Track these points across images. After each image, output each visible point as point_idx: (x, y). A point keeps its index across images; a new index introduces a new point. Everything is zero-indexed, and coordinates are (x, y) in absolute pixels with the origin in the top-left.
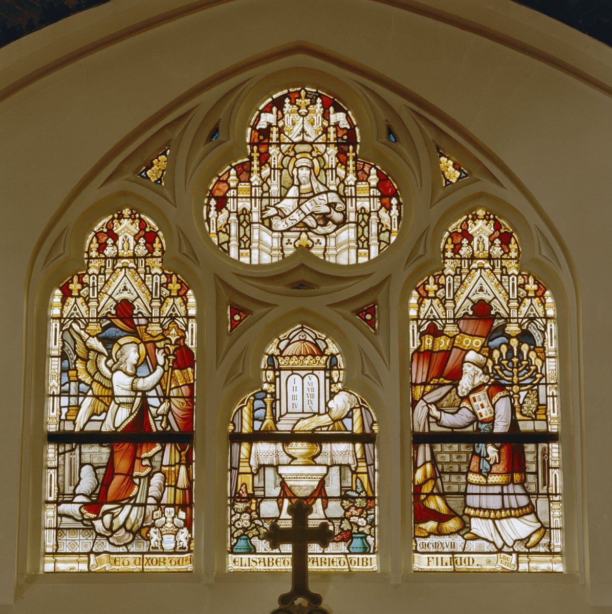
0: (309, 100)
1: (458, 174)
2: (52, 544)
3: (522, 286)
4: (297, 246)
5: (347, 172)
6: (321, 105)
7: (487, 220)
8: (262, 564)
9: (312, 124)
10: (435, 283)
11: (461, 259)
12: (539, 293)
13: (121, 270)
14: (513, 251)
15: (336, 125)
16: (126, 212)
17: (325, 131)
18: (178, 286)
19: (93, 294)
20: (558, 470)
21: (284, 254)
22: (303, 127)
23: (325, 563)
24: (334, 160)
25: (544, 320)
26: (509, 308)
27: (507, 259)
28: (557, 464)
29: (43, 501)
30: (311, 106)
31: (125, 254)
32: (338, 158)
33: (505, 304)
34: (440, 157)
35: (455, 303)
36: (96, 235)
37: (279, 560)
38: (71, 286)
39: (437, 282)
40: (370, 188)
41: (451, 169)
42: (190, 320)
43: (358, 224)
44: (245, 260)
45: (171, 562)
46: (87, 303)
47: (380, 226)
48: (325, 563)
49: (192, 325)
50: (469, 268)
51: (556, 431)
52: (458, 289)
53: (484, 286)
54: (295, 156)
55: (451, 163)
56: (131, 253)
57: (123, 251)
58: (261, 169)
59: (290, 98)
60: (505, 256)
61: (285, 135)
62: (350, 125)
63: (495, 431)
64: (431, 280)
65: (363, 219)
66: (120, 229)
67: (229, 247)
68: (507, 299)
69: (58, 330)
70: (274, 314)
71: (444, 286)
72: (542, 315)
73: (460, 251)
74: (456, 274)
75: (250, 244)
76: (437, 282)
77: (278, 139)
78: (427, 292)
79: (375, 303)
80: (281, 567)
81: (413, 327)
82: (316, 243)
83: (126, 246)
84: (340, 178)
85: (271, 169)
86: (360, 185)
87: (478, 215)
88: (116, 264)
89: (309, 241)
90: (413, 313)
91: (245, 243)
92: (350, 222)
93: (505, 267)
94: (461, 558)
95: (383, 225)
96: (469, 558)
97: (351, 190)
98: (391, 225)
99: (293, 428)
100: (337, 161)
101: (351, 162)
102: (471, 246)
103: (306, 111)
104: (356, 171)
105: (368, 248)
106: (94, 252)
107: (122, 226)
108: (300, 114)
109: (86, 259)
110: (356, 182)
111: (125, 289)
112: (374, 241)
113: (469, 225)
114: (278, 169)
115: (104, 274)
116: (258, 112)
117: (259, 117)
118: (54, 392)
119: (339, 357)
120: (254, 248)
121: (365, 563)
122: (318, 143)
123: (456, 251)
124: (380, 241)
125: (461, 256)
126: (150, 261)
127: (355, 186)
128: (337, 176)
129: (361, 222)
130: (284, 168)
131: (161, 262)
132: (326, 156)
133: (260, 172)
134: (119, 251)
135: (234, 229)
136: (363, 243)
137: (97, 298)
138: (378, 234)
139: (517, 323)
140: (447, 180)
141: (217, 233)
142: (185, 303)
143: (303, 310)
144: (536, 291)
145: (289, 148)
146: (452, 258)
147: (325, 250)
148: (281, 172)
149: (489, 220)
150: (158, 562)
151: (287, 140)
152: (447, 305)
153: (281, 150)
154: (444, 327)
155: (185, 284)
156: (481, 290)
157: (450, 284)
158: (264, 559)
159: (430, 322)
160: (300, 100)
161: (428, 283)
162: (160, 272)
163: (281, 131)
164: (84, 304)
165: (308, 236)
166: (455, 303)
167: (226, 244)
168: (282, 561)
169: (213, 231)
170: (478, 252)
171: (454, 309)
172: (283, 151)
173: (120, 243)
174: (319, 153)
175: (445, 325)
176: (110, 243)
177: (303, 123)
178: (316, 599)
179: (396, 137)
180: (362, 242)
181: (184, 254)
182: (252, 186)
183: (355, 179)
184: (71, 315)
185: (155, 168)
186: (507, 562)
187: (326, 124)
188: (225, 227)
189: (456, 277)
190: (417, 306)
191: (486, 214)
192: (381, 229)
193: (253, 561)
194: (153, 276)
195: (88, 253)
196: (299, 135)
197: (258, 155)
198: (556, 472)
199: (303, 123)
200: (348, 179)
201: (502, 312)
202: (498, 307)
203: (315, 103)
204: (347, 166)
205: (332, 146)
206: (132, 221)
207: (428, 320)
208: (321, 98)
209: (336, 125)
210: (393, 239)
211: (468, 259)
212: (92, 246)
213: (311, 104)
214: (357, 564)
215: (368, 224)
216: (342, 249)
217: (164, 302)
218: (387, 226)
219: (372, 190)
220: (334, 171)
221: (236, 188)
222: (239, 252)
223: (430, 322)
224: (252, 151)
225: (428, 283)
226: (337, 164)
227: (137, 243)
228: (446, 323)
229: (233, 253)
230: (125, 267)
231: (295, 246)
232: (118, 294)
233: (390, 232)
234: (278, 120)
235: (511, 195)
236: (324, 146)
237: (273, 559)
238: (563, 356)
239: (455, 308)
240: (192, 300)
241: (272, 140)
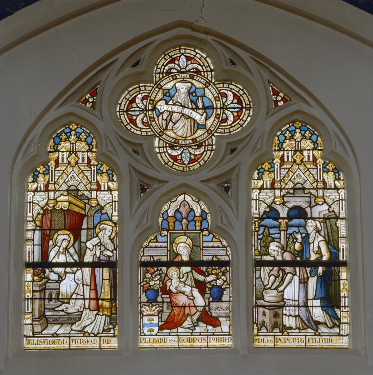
8: (46, 343)
23: (221, 341)
37: (55, 341)
45: (59, 342)
48: (221, 341)
63: (323, 260)
70: (164, 188)
79: (230, 179)
96: (165, 338)
118: (344, 295)
143: (184, 185)
150: (54, 342)
158: (217, 338)
168: (58, 341)
193: (40, 342)
214: (62, 343)
235: (316, 111)
237: (296, 339)
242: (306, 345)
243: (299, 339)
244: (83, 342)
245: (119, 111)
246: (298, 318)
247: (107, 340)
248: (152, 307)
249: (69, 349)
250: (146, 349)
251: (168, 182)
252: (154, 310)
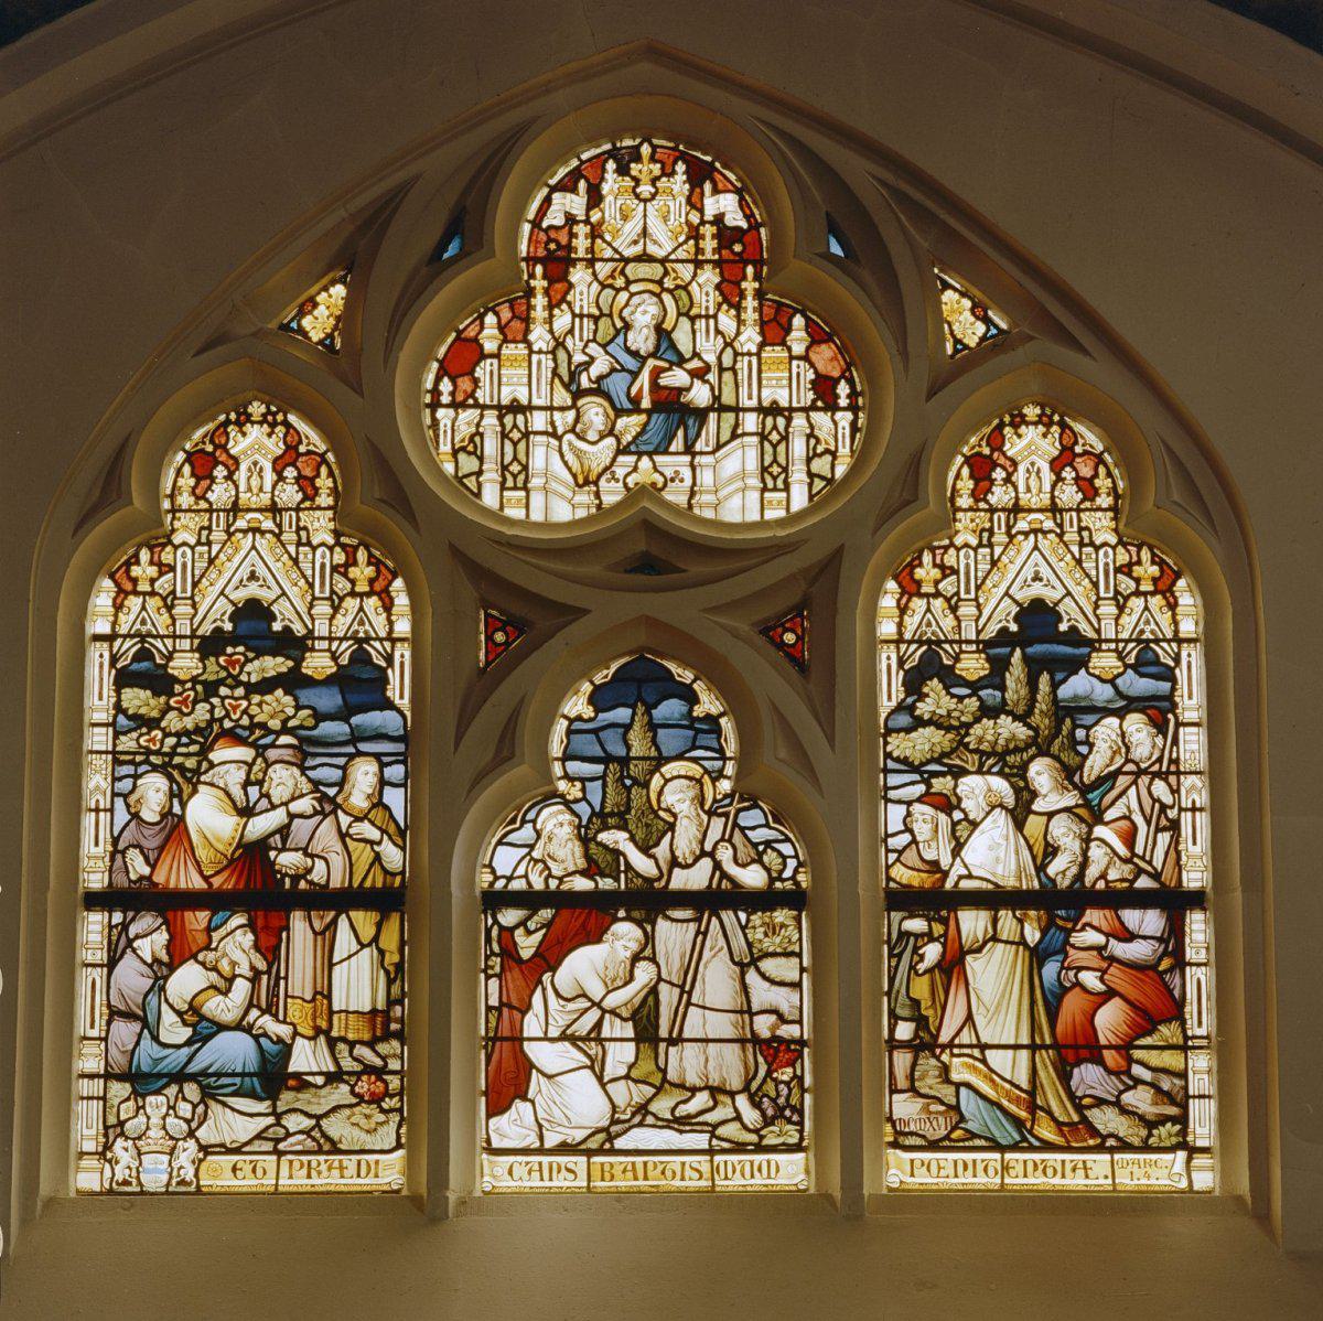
0: (659, 166)
1: (981, 328)
2: (93, 1132)
3: (1126, 569)
4: (631, 485)
5: (740, 322)
6: (684, 177)
7: (1044, 425)
8: (630, 1175)
9: (665, 219)
10: (152, 563)
11: (210, 511)
12: (377, 587)
13: (1026, 538)
14: (324, 491)
15: (719, 219)
16: (257, 409)
17: (694, 234)
18: (370, 571)
19: (968, 591)
20: (1203, 968)
21: (601, 503)
22: (645, 223)
24: (711, 298)
25: (387, 645)
26: (1097, 616)
27: (311, 509)
28: (1202, 957)
30: (664, 179)
31: (255, 502)
32: (722, 294)
33: (1089, 610)
34: (943, 291)
35: (194, 606)
36: (190, 457)
38: (919, 573)
39: (938, 561)
40: (791, 358)
41: (967, 316)
42: (399, 645)
43: (763, 437)
44: (515, 513)
45: (986, 1170)
46: (954, 609)
47: (813, 441)
48: (319, 1173)
49: (402, 656)
50: (1008, 533)
51: (1199, 884)
52: (202, 576)
53: (1041, 570)
54: (626, 288)
55: (967, 303)
56: (265, 499)
57: (249, 495)
58: (551, 316)
59: (617, 161)
60: (1087, 504)
61: (604, 241)
62: (749, 221)
64: (144, 555)
65: (775, 427)
66: (1019, 447)
67: (479, 485)
68: (1094, 598)
69: (894, 667)
71: (172, 569)
72: (383, 634)
73: (989, 497)
74: (980, 545)
75: (526, 481)
76: (938, 561)
77: (591, 250)
78: (135, 581)
81: (889, 658)
82: (672, 480)
83: (255, 482)
84: (724, 337)
85: (574, 315)
86: (768, 352)
87: (251, 415)
88: (235, 521)
89: (657, 475)
90: (887, 628)
91: (515, 477)
92: (744, 434)
93: (1087, 528)
94: (752, 1163)
95: (818, 442)
96: (726, 1162)
97: (750, 362)
98: (836, 441)
100: (720, 299)
101: (750, 303)
102: (234, 482)
103: (653, 190)
104: (763, 325)
105: (787, 488)
106: (185, 494)
107: (1025, 441)
108: (637, 196)
109: (169, 511)
110: (761, 346)
111: (253, 576)
112: (798, 475)
113: (231, 436)
114: (589, 316)
115: (209, 543)
116: (545, 191)
117: (547, 201)
118: (1194, 802)
119: (723, 721)
120: (535, 489)
122: (677, 261)
123: (979, 494)
124: (811, 475)
125: (211, 504)
126: (1088, 519)
127: (758, 354)
128: (718, 332)
129: (770, 433)
130: (602, 315)
131: (334, 519)
132: (694, 288)
133: (550, 320)
134: (241, 495)
135: (490, 446)
136: (775, 478)
137: (192, 598)
138: (809, 460)
139: (1116, 650)
140: (957, 341)
141: (455, 453)
142: (388, 607)
144: (1155, 580)
145: (614, 271)
146: (971, 509)
147: (692, 494)
148: (596, 324)
149: (1048, 425)
151: (609, 253)
152: (961, 611)
153: (594, 274)
154: (957, 659)
155: (386, 567)
156: (1037, 578)
157: (184, 566)
158: (540, 1164)
159: (925, 648)
160: (640, 166)
161: (138, 563)
162: (1113, 540)
163: (595, 233)
164: (948, 612)
165: (654, 463)
166: (194, 606)
167: (473, 478)
169: (445, 448)
170: (1029, 495)
171: (977, 620)
172: (601, 277)
173: (1020, 477)
174: (679, 282)
175: (958, 655)
176: (1069, 477)
177: (645, 216)
179: (842, 243)
180: (772, 475)
181: (1176, 503)
182: (531, 351)
183: (759, 339)
184: (921, 636)
185: (321, 311)
186: (571, 1175)
187: (695, 218)
188: (471, 440)
189: (199, 549)
190: (897, 612)
191: (269, 412)
192: (815, 448)
193: (569, 1170)
194: (314, 549)
195: (172, 497)
196: (635, 242)
197: (757, 285)
198: (1201, 973)
199: (645, 216)
200: (742, 338)
201: (1084, 627)
202: (1071, 616)
203: (673, 173)
204: (738, 307)
205: (708, 267)
206: (269, 430)
207: (921, 643)
208: (684, 162)
209: (719, 219)
210: (840, 471)
211: (1009, 511)
212: (959, 484)
213: (664, 174)
214: (1059, 1174)
215: (785, 438)
216: (727, 488)
217: (339, 606)
218: (827, 443)
219: (795, 363)
220: (712, 322)
221: (497, 356)
222: (502, 496)
223: (925, 648)
224: (532, 276)
225: (138, 563)
226: (720, 305)
227: (281, 478)
228: (962, 652)
229: (490, 498)
230: (1035, 531)
231: (625, 485)
232: (237, 588)
233: (834, 454)
234: (589, 208)
236: (691, 267)
237: (319, 1173)
238: (1214, 723)
239: (194, 616)
240: (402, 601)
241: (703, 254)
243: (978, 1162)
244: (986, 1170)
246: (749, 1046)
249: (1114, 1190)
251: (585, 612)
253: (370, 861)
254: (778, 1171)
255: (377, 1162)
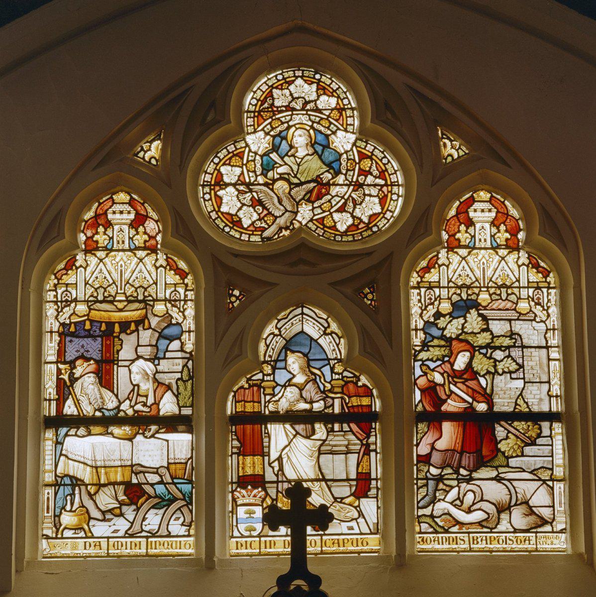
29: (43, 361)
45: (362, 543)
80: (280, 549)
99: (144, 484)
121: (475, 542)
158: (486, 537)
178: (315, 581)
193: (510, 540)
242: (147, 552)
244: (362, 543)
245: (203, 186)
247: (116, 543)
248: (251, 492)
250: (499, 553)
252: (255, 496)
253: (521, 322)
254: (275, 545)
255: (456, 537)
